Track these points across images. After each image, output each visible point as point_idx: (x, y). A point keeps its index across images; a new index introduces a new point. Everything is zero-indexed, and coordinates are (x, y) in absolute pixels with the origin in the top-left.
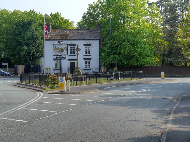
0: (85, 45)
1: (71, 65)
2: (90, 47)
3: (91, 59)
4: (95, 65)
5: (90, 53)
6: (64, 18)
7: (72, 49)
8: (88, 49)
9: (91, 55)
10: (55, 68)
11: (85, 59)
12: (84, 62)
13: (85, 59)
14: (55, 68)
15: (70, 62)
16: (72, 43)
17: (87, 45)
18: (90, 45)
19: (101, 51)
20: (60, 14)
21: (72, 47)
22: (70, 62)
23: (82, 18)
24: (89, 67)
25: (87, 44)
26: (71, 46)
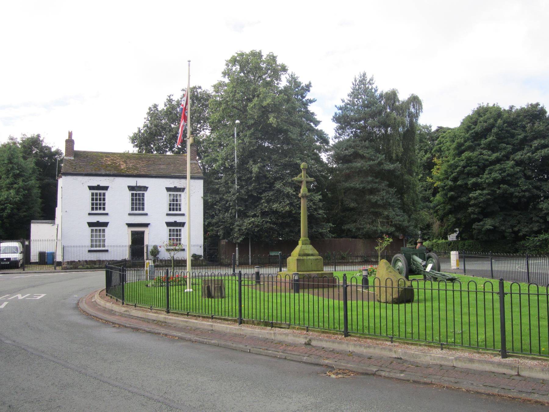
0: (168, 189)
1: (132, 239)
2: (180, 195)
3: (149, 224)
4: (16, 244)
5: (104, 209)
6: (155, 106)
7: (136, 199)
8: (177, 201)
9: (107, 214)
10: (92, 246)
11: (169, 224)
12: (166, 229)
13: (169, 224)
14: (170, 245)
15: (132, 231)
16: (138, 185)
17: (176, 189)
18: (182, 190)
19: (208, 207)
20: (183, 90)
21: (136, 194)
22: (132, 231)
23: (542, 108)
24: (104, 246)
25: (175, 187)
26: (134, 192)
